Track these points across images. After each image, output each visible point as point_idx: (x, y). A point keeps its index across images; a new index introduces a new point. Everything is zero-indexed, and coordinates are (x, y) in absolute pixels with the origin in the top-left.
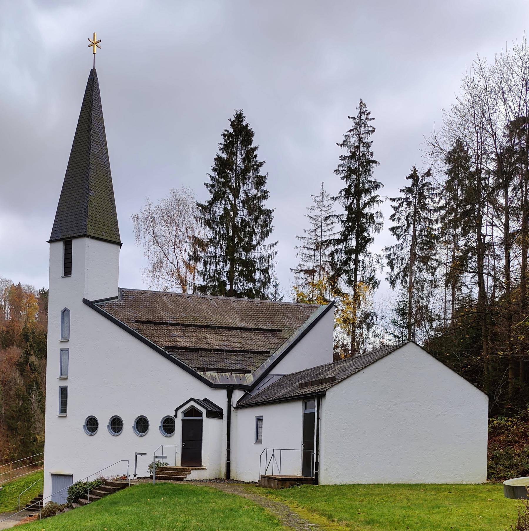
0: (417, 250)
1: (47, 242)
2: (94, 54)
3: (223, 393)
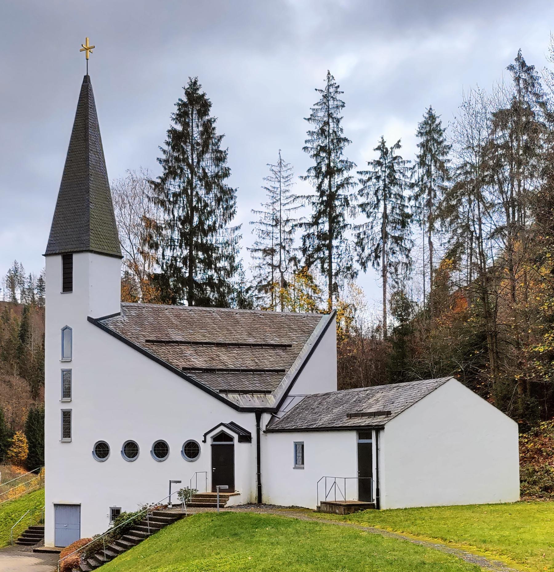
0: (388, 229)
1: (43, 255)
3: (253, 416)
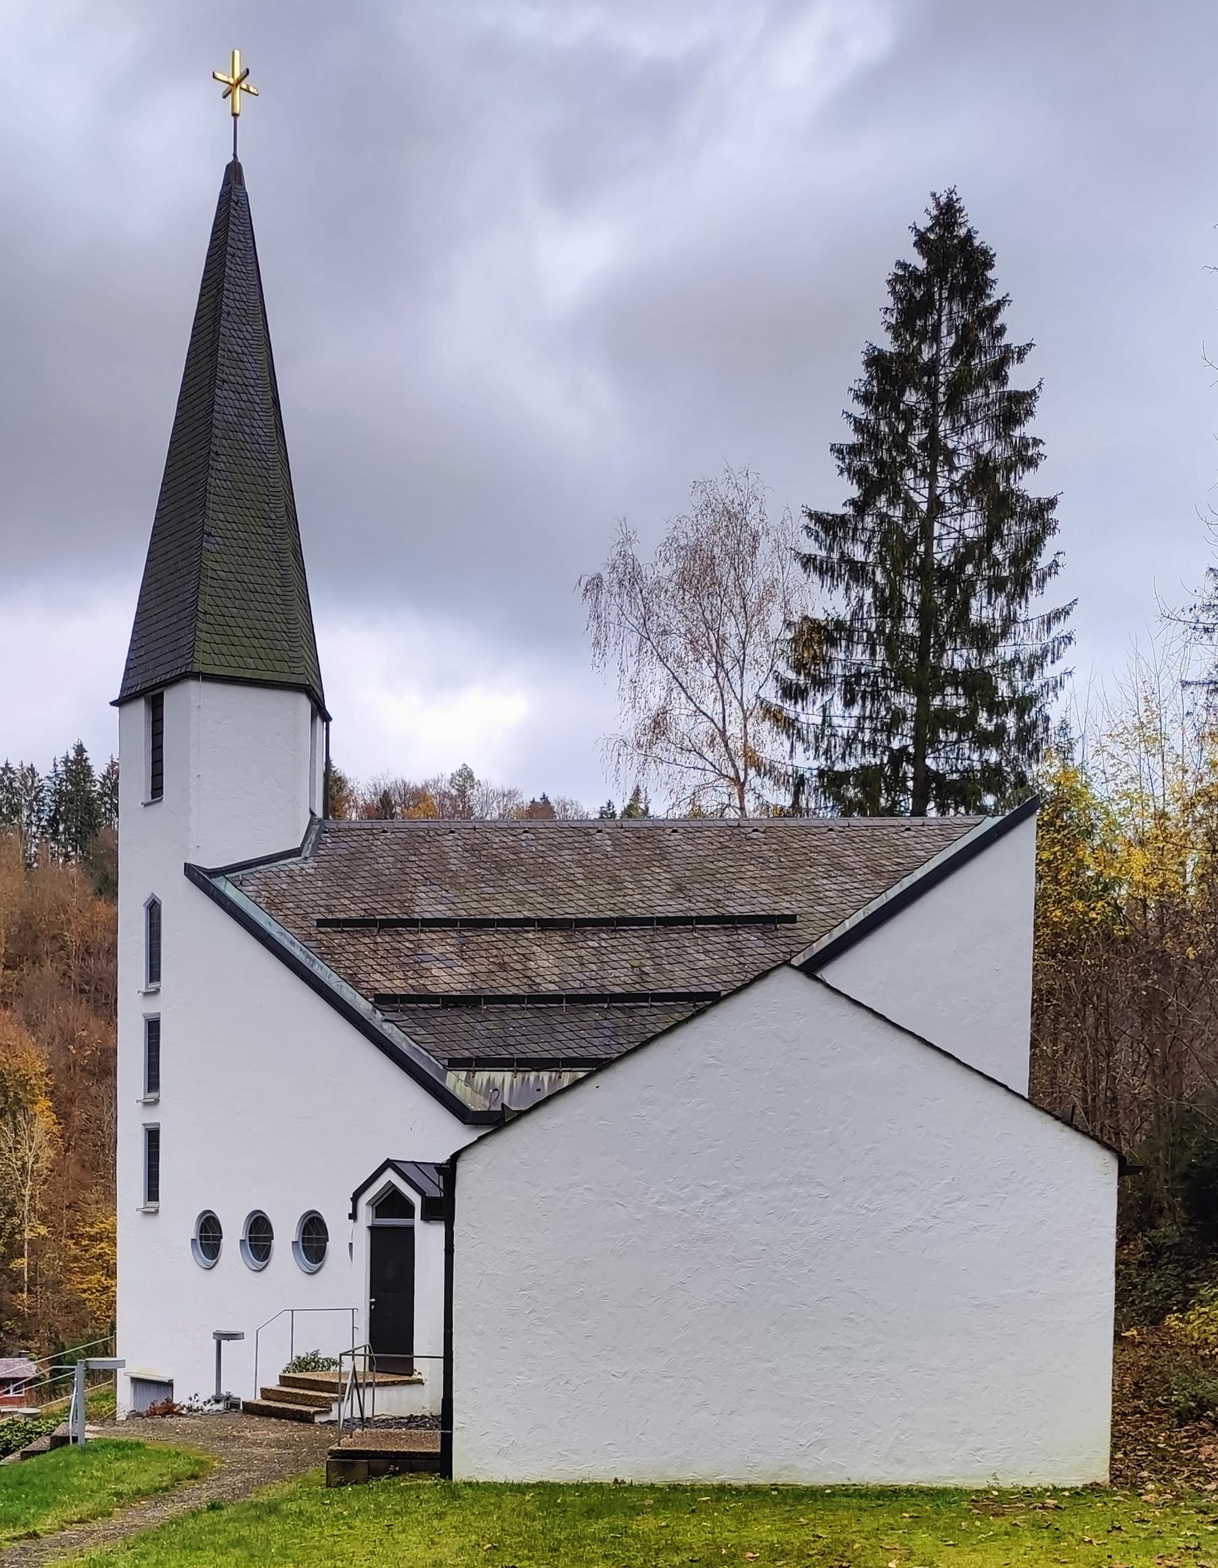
2: (235, 115)
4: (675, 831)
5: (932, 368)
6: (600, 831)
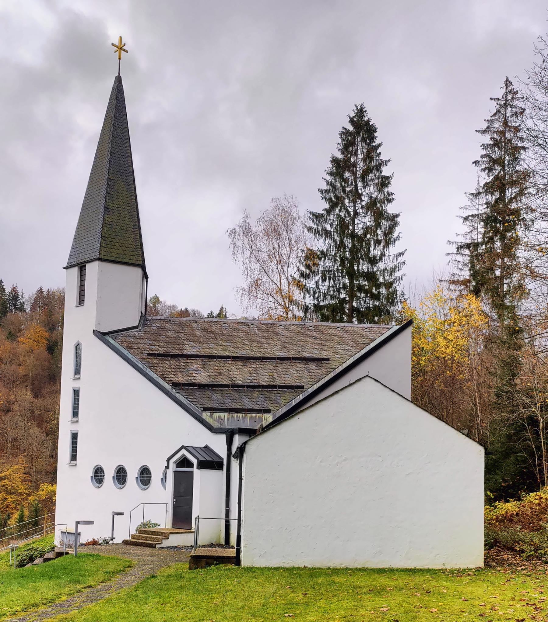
4: (281, 325)
5: (355, 165)
6: (252, 324)
